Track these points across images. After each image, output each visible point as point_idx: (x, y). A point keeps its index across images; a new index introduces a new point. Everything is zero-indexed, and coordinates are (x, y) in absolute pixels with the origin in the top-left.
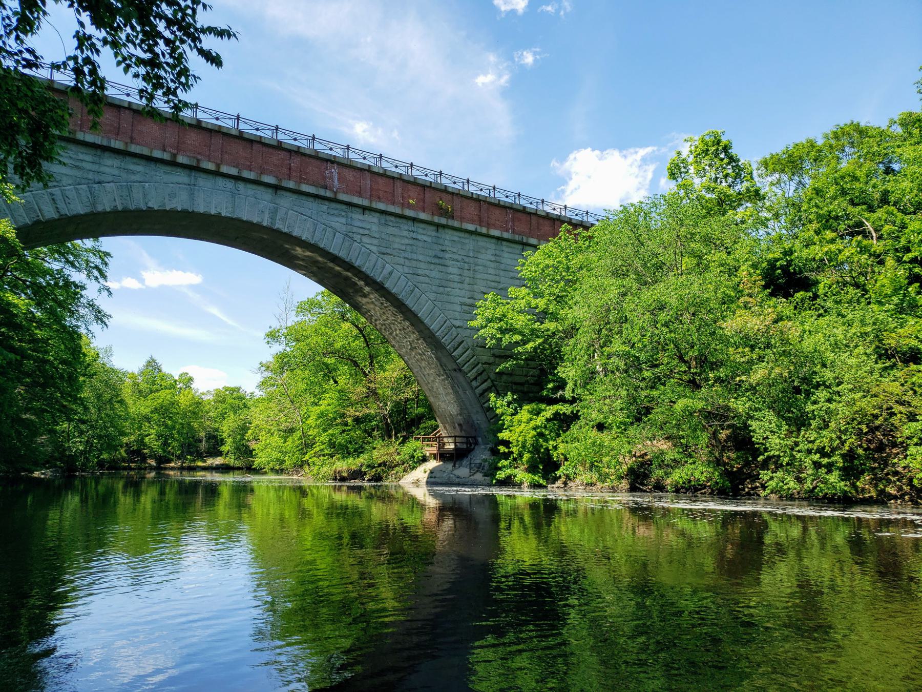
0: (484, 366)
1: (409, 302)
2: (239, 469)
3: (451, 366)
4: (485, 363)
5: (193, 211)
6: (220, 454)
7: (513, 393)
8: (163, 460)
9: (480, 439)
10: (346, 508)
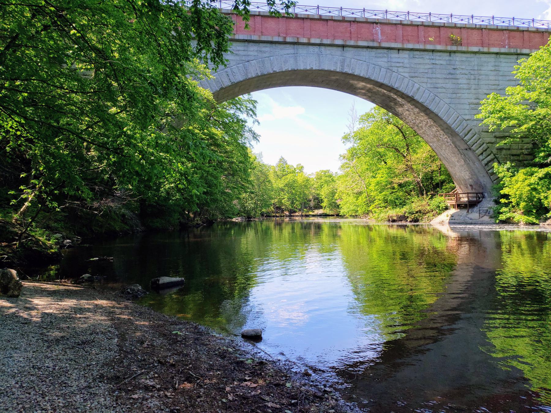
0: (488, 145)
1: (432, 107)
3: (463, 146)
6: (321, 207)
7: (512, 161)
8: (292, 212)
9: (486, 195)
10: (397, 237)
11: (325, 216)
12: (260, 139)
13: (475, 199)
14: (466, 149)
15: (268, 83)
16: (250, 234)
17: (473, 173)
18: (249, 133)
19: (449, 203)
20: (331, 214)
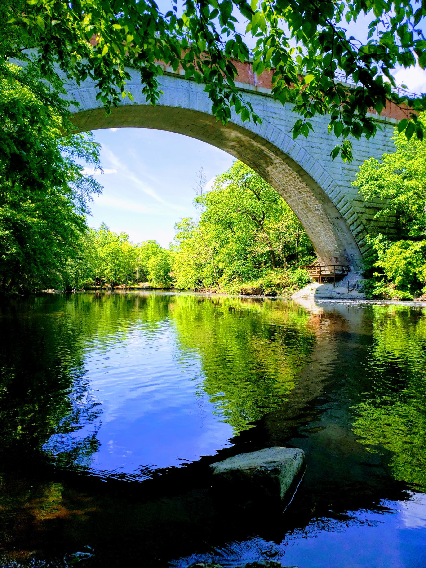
0: (359, 214)
1: (307, 168)
2: (158, 289)
3: (334, 214)
4: (359, 213)
5: (163, 106)
6: (147, 280)
7: (383, 234)
8: (115, 284)
9: (352, 268)
10: (249, 312)
11: (152, 289)
12: (103, 191)
13: (340, 272)
14: (337, 218)
15: (122, 120)
16: (70, 306)
17: (340, 244)
18: (88, 183)
19: (310, 277)
20: (157, 287)
